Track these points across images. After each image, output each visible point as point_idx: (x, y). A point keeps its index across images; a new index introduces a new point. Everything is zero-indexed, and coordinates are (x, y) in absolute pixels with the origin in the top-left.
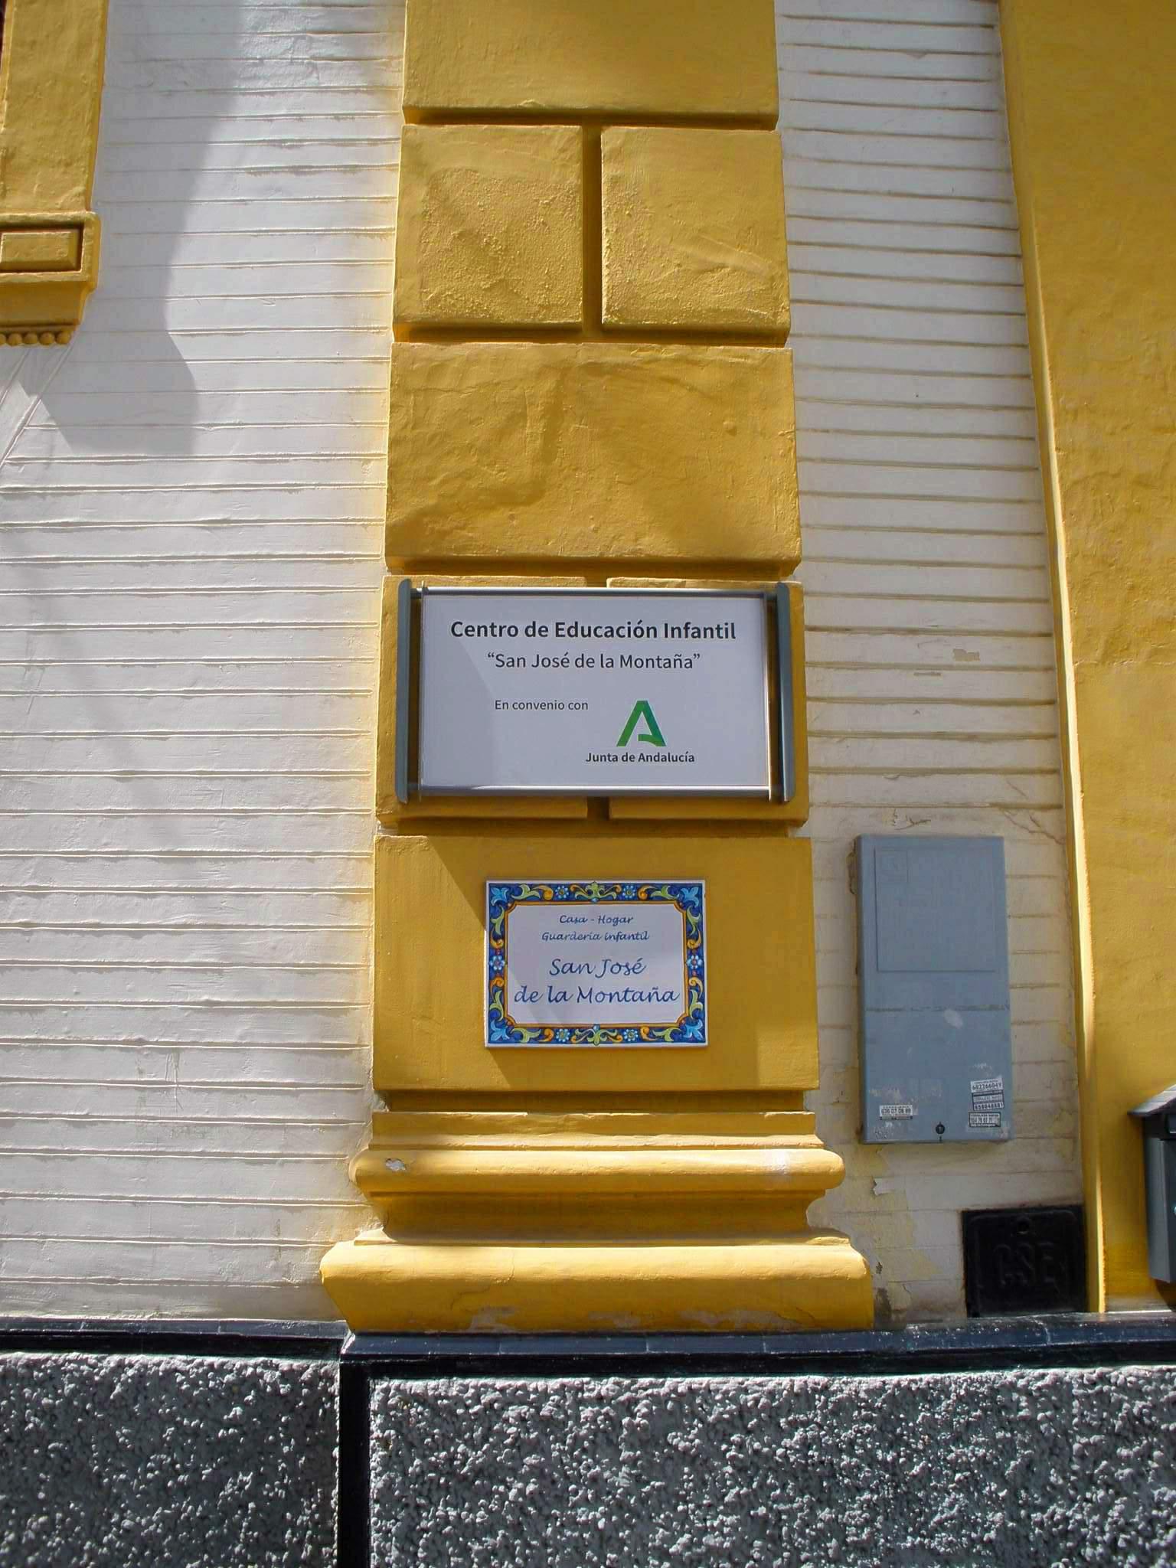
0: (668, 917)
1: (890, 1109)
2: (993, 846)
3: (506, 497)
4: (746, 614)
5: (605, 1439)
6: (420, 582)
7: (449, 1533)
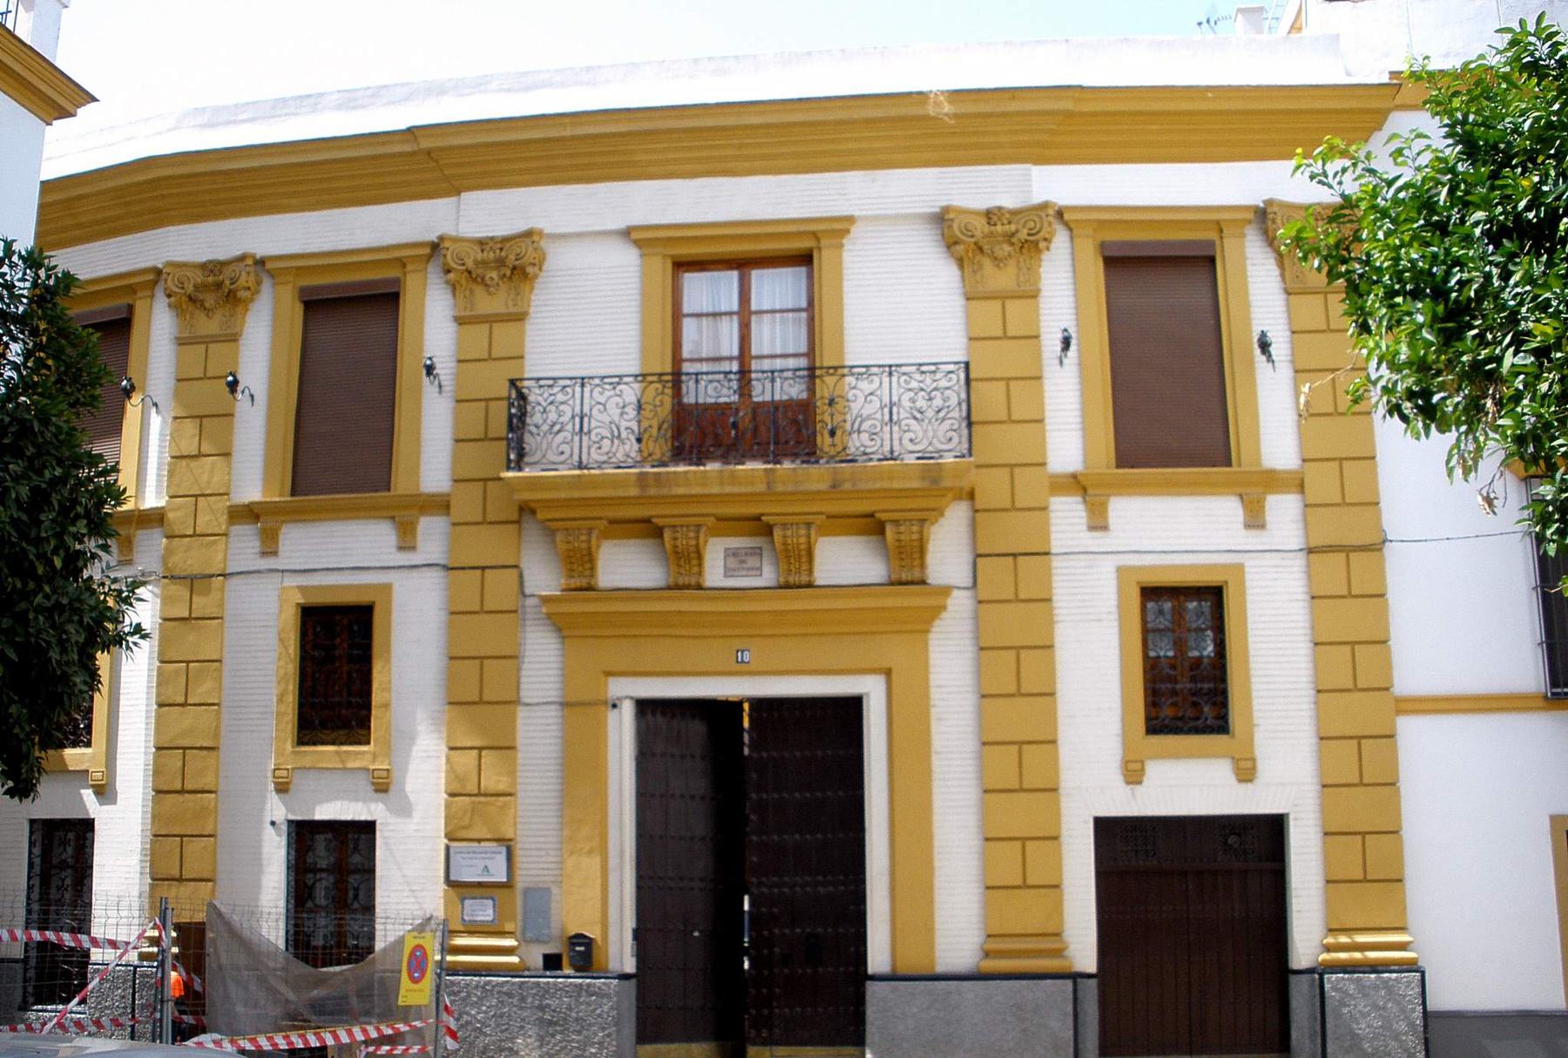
0: (490, 902)
1: (529, 935)
2: (548, 889)
3: (464, 828)
4: (504, 850)
5: (476, 987)
6: (453, 844)
7: (64, 562)
